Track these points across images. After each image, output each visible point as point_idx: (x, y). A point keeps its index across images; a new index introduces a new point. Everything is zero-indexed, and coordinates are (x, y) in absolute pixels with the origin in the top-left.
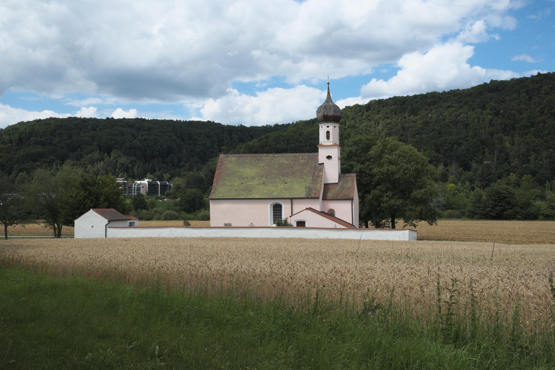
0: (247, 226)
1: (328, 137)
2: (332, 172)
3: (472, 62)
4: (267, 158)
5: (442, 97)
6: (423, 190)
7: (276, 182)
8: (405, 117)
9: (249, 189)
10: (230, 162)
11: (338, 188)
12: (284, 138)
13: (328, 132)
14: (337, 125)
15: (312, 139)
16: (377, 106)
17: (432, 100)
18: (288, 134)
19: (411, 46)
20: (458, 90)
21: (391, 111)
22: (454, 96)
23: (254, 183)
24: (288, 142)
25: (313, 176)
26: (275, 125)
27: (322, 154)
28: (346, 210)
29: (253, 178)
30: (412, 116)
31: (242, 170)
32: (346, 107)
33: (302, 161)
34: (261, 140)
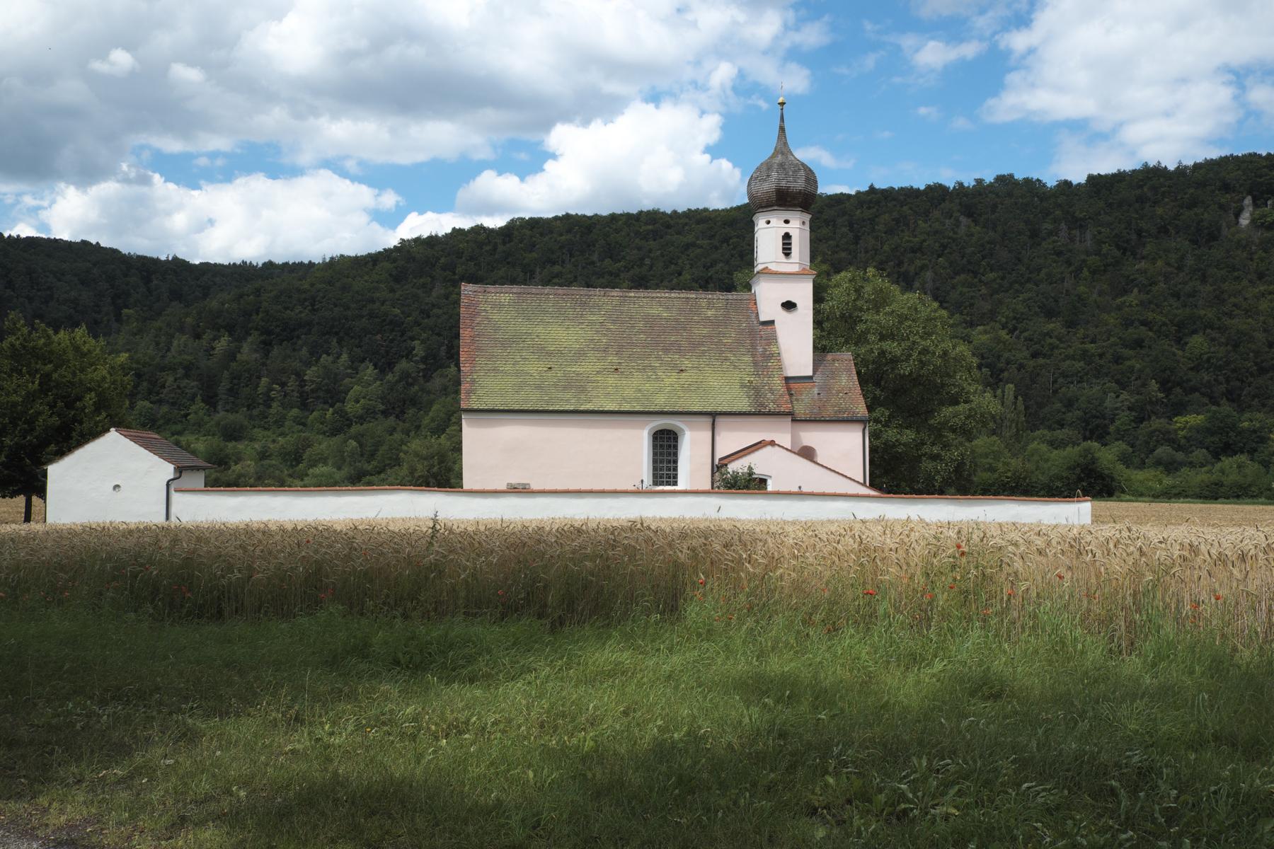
0: (631, 488)
1: (787, 251)
2: (796, 345)
3: (714, 151)
4: (607, 301)
5: (672, 222)
6: (960, 408)
7: (653, 369)
8: (593, 263)
9: (578, 385)
10: (500, 306)
11: (816, 391)
12: (304, 296)
13: (787, 237)
14: (807, 217)
15: (372, 301)
16: (528, 232)
17: (650, 227)
18: (312, 285)
19: (591, 106)
20: (706, 210)
21: (561, 247)
22: (698, 222)
23: (587, 367)
24: (313, 305)
25: (753, 356)
26: (264, 264)
27: (768, 297)
28: (846, 448)
29: (580, 355)
30: (608, 261)
31: (540, 329)
32: (454, 229)
33: (710, 313)
34: (241, 296)
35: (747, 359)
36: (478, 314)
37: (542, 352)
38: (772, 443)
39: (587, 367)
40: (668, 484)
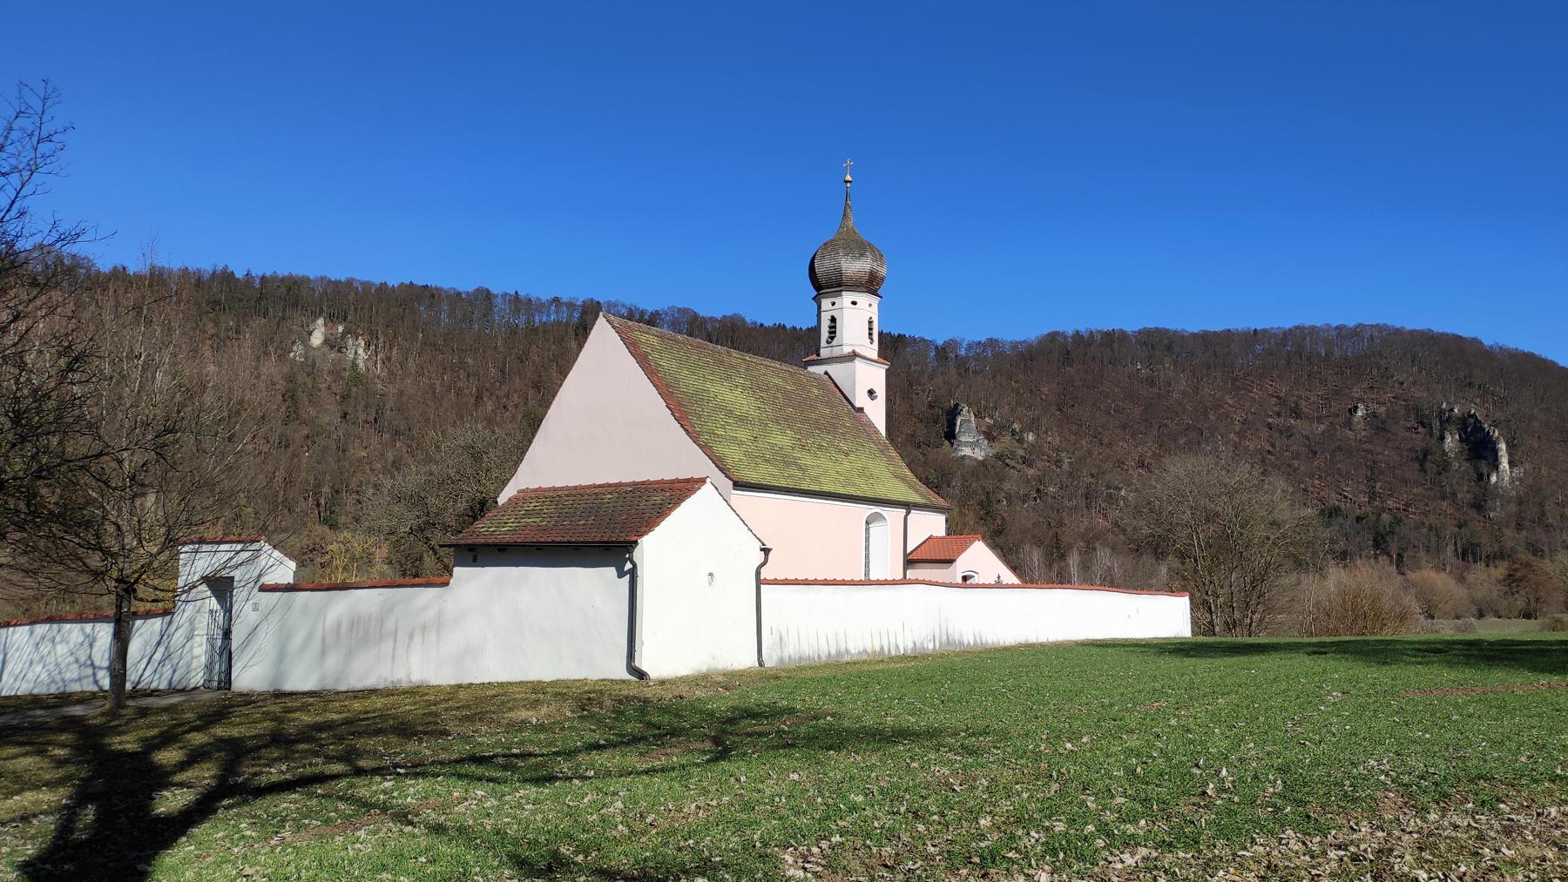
13: (870, 322)
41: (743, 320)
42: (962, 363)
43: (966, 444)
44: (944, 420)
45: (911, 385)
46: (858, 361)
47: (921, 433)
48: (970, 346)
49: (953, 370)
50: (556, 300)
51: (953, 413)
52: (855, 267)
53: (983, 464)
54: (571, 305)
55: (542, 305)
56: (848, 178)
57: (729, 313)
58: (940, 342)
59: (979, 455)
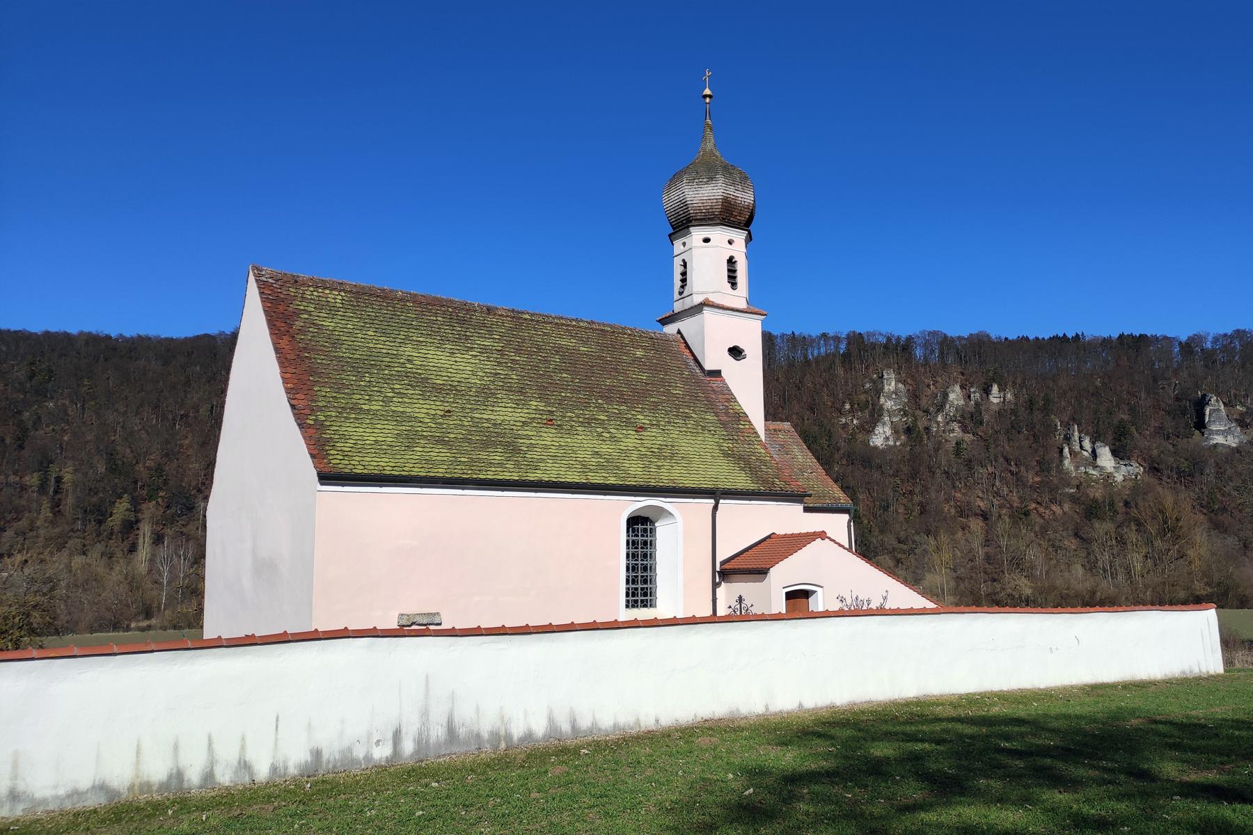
9: (493, 438)
13: (731, 261)
29: (486, 395)
31: (408, 350)
35: (710, 417)
36: (297, 314)
37: (424, 384)
38: (822, 535)
39: (506, 413)
40: (645, 604)
41: (988, 336)
42: (1209, 356)
43: (1218, 432)
44: (1191, 410)
45: (1155, 381)
46: (707, 313)
47: (1169, 425)
48: (1216, 340)
49: (1199, 364)
50: (824, 335)
51: (1202, 403)
52: (704, 194)
53: (1237, 450)
54: (837, 339)
55: (813, 341)
56: (707, 91)
57: (975, 331)
58: (1184, 338)
59: (1232, 442)
